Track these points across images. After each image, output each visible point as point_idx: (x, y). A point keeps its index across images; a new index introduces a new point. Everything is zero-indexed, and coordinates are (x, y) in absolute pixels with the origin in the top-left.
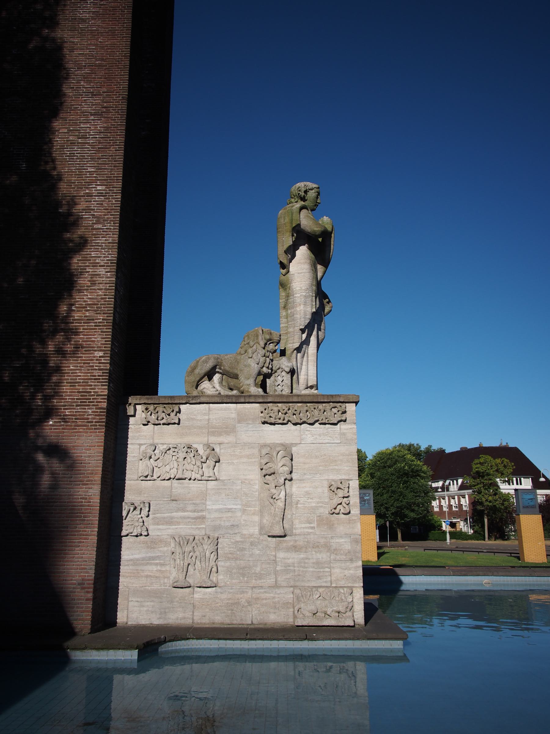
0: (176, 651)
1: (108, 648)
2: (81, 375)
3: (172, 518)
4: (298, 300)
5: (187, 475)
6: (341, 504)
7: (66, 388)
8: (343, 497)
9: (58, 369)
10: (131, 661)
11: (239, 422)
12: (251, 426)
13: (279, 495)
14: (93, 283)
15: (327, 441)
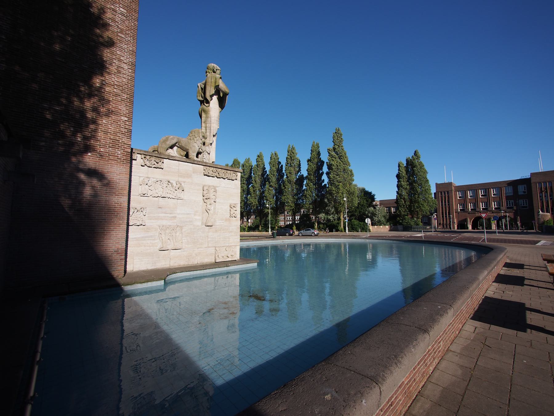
0: (171, 279)
1: (148, 281)
2: (112, 128)
3: (159, 217)
4: (213, 121)
5: (168, 195)
7: (100, 135)
9: (94, 122)
10: (160, 286)
11: (193, 173)
14: (119, 72)
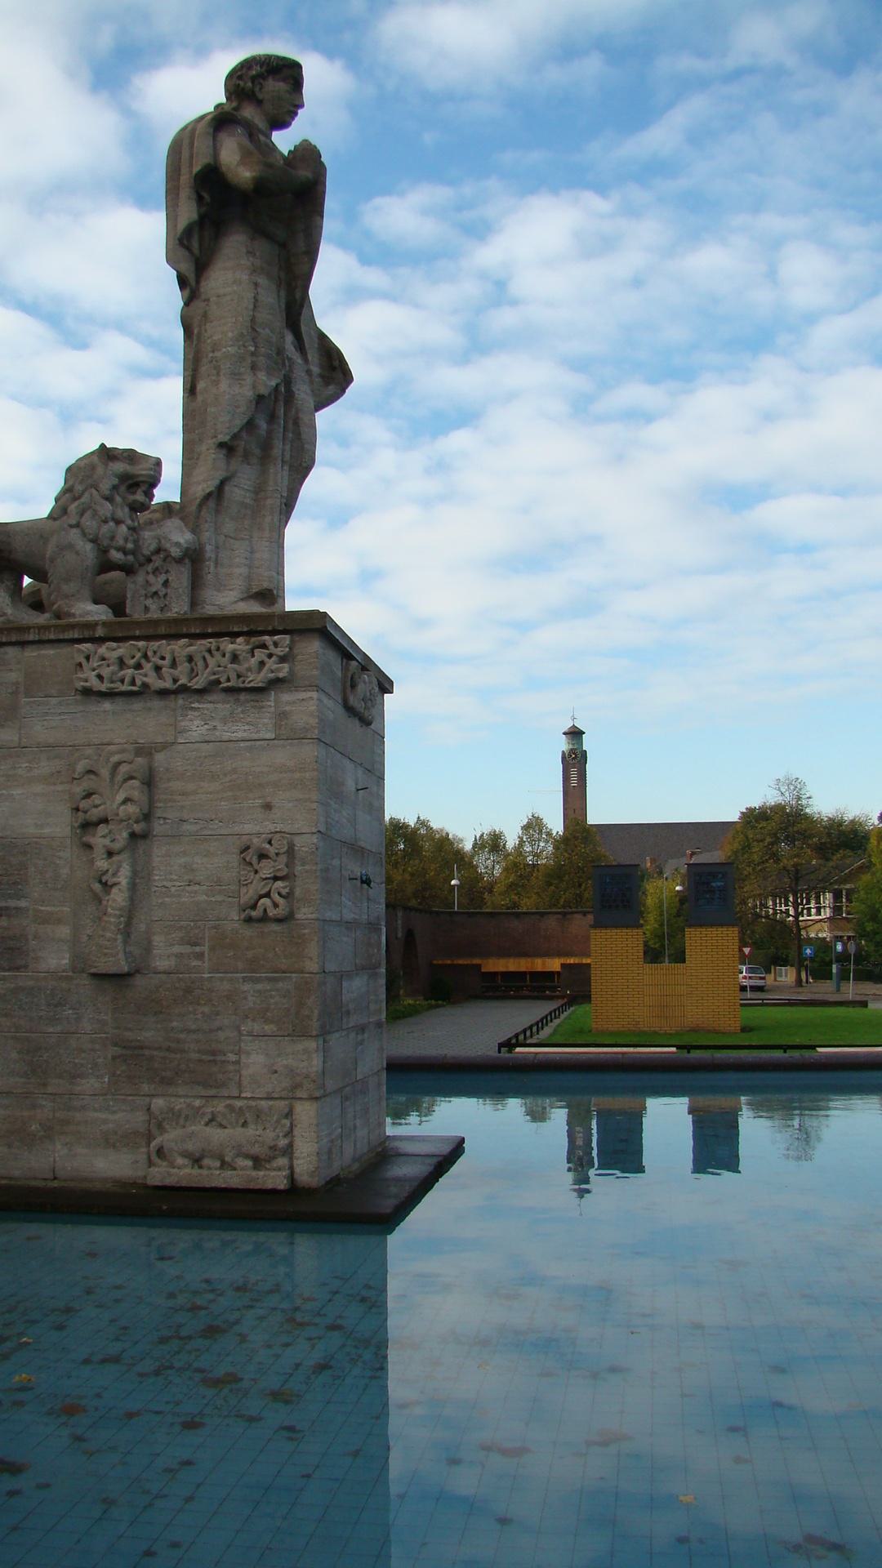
6: (268, 895)
8: (276, 879)
12: (54, 701)
13: (114, 875)
15: (240, 735)
